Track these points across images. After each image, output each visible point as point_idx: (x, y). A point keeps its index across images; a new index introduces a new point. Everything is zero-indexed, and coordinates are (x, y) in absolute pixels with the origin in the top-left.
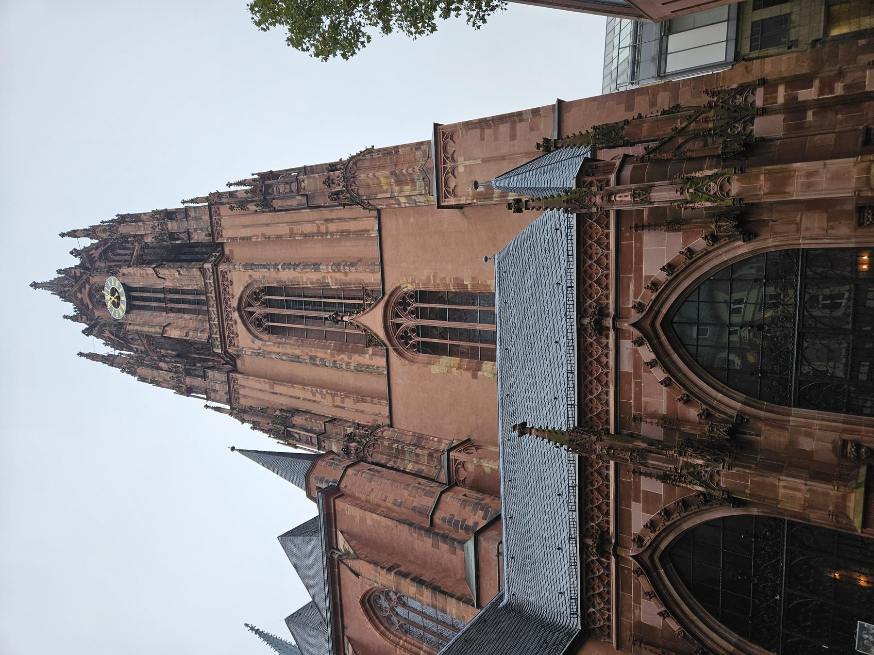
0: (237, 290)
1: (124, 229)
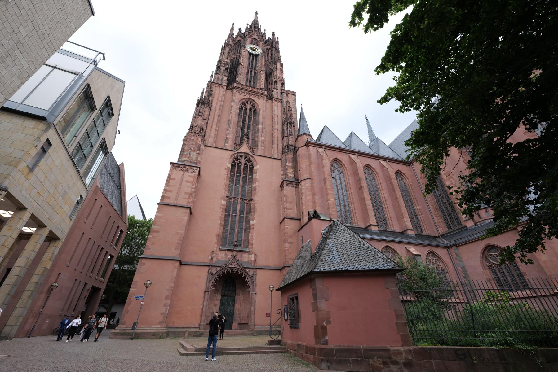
0: (256, 100)
1: (278, 64)
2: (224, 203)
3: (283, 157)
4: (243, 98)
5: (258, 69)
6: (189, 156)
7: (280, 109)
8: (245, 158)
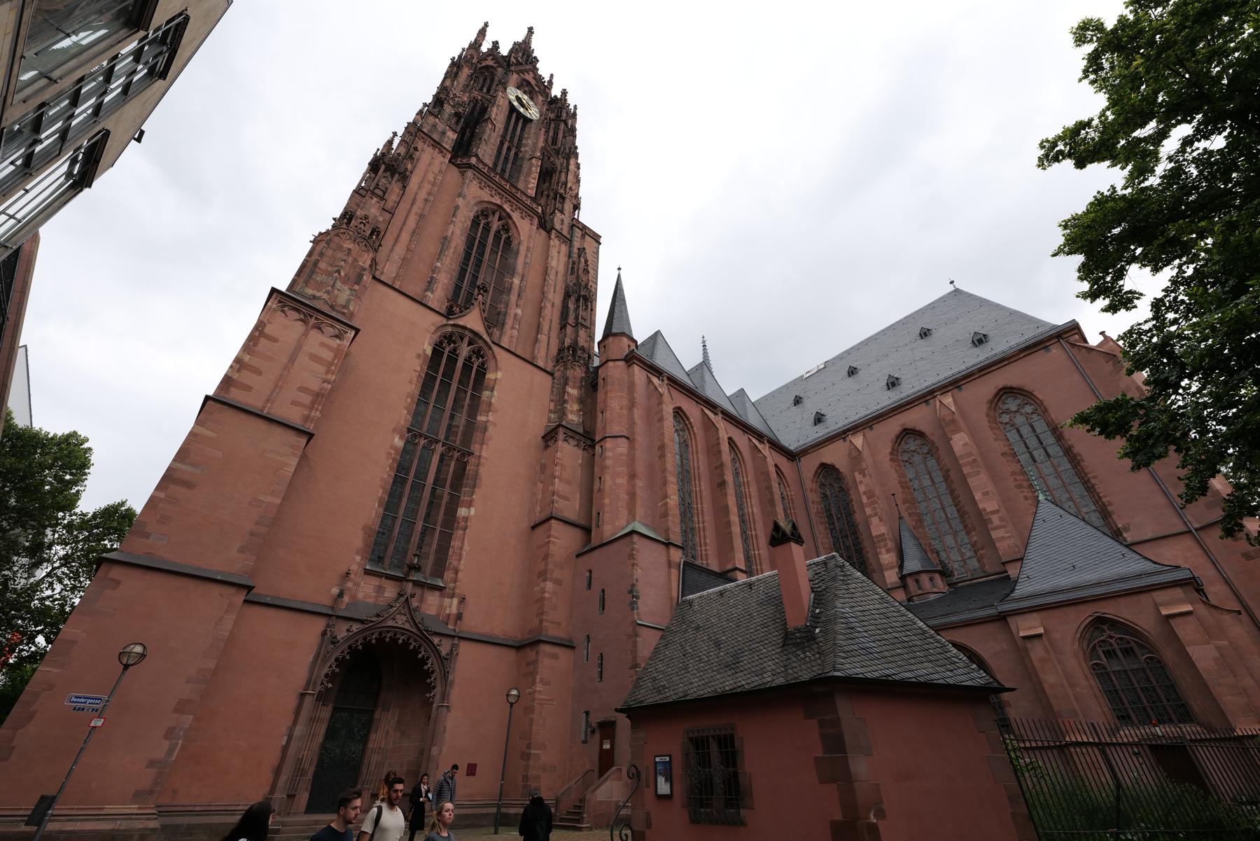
0: (516, 216)
1: (572, 162)
2: (399, 442)
3: (559, 370)
4: (486, 200)
5: (526, 151)
6: (330, 288)
7: (563, 259)
8: (470, 344)
